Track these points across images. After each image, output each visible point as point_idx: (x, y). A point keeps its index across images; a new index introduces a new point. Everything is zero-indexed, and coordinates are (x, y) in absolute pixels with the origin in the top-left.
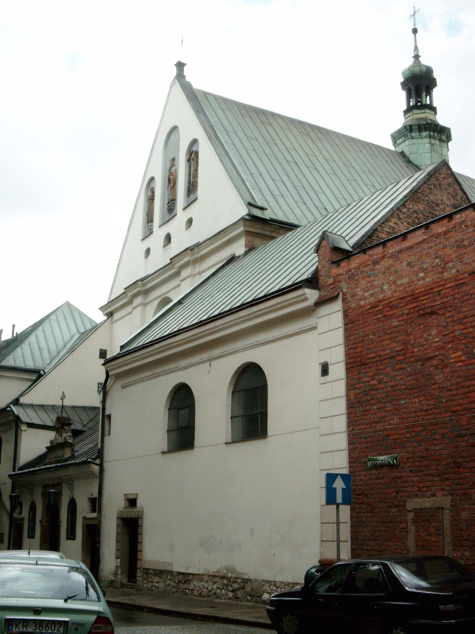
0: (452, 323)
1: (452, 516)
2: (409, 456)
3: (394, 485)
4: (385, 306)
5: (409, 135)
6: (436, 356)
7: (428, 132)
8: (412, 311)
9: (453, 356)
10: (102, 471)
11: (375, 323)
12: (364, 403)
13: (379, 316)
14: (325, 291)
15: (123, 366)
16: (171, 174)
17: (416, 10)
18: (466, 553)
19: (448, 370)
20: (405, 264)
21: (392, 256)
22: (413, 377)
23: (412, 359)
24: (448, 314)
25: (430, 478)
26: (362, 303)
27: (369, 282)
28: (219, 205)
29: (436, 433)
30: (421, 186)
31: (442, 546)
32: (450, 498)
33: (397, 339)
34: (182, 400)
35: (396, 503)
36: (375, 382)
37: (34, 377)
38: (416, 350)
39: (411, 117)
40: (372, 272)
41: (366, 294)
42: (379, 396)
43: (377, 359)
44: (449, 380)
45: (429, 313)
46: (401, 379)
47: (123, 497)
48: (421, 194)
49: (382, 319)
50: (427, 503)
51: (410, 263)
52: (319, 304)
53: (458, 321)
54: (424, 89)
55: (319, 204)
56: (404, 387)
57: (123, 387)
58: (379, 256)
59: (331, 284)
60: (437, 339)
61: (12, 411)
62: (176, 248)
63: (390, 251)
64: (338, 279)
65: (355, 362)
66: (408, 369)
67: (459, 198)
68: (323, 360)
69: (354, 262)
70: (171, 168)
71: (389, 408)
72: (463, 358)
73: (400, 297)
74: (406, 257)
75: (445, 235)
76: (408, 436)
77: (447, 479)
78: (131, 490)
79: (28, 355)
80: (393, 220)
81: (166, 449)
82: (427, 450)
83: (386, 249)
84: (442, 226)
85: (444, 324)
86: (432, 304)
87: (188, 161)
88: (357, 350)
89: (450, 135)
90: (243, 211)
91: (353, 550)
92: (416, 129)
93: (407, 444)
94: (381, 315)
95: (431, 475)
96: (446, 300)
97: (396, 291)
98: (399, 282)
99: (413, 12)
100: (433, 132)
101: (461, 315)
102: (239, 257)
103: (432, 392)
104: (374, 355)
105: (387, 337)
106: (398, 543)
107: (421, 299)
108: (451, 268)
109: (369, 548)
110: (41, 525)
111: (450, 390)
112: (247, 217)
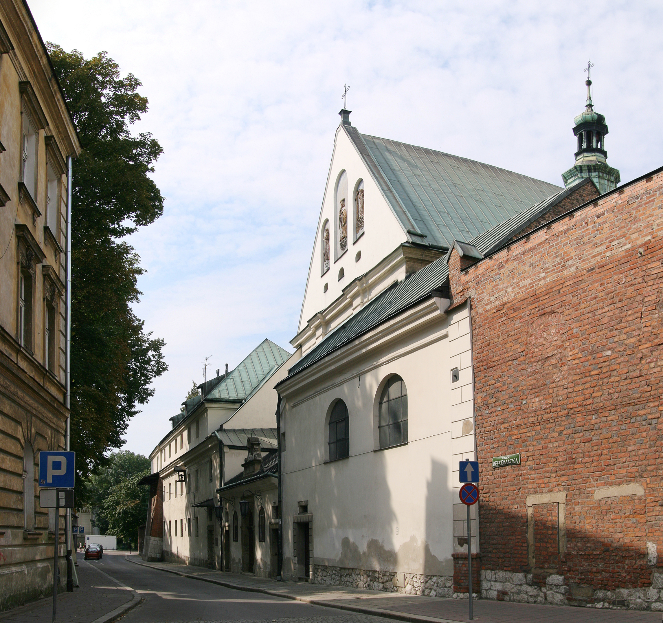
0: (570, 321)
1: (566, 510)
3: (516, 482)
4: (508, 309)
6: (555, 354)
7: (597, 173)
9: (570, 353)
10: (280, 482)
11: (500, 326)
12: (490, 405)
13: (503, 319)
15: (291, 387)
16: (342, 213)
17: (591, 64)
18: (579, 544)
19: (565, 368)
21: (516, 259)
22: (533, 377)
23: (533, 360)
25: (547, 475)
26: (488, 307)
29: (553, 431)
30: (562, 200)
31: (557, 539)
33: (520, 341)
34: (339, 414)
35: (517, 500)
36: (499, 384)
39: (582, 159)
40: (498, 276)
41: (492, 298)
43: (502, 361)
44: (566, 378)
45: (550, 312)
46: (523, 379)
47: (297, 504)
48: (562, 207)
49: (505, 322)
51: (533, 263)
53: (576, 319)
56: (525, 387)
58: (504, 259)
59: (460, 292)
60: (555, 339)
61: (216, 436)
62: (347, 280)
63: (514, 254)
65: (482, 366)
66: (529, 370)
69: (481, 268)
70: (342, 208)
71: (512, 409)
72: (579, 355)
73: (522, 299)
75: (565, 233)
76: (528, 435)
78: (302, 498)
81: (328, 459)
83: (510, 252)
84: (562, 225)
85: (563, 322)
86: (552, 304)
87: (356, 200)
89: (619, 176)
91: (481, 544)
92: (585, 170)
93: (528, 443)
94: (505, 318)
96: (564, 298)
97: (518, 293)
98: (521, 284)
99: (588, 66)
100: (602, 173)
104: (498, 358)
105: (510, 339)
106: (519, 537)
107: (541, 299)
108: (570, 266)
109: (495, 542)
110: (242, 531)
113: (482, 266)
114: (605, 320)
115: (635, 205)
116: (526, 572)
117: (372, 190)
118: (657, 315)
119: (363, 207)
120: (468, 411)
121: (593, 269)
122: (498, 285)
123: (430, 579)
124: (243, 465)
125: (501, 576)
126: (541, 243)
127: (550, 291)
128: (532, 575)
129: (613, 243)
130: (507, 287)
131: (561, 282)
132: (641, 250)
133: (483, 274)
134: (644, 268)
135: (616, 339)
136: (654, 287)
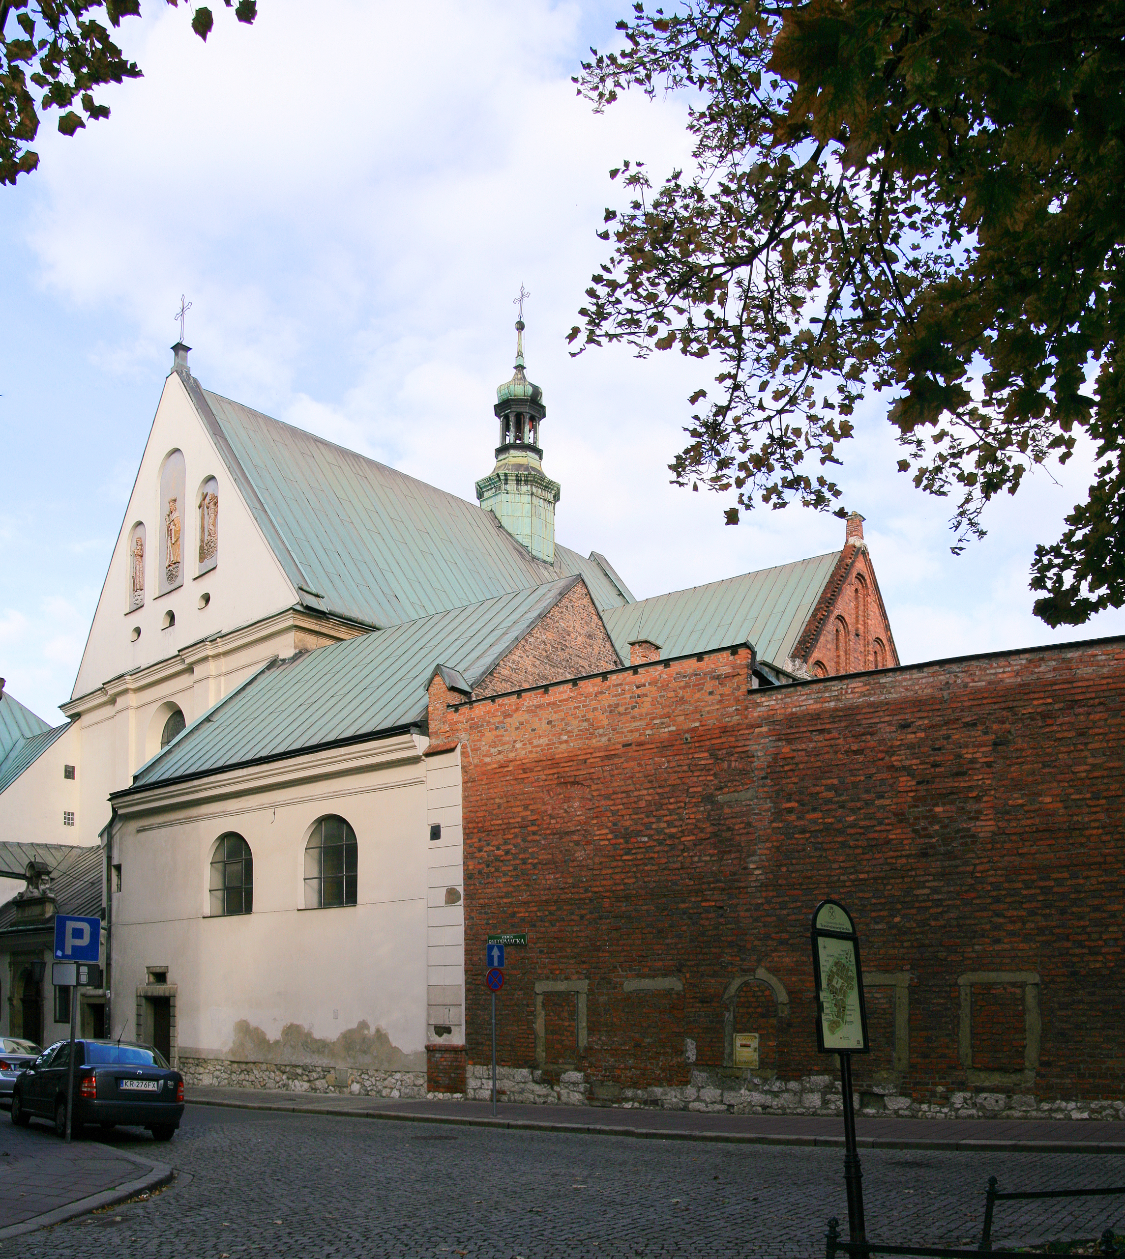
2: (540, 935)
5: (503, 486)
8: (550, 777)
14: (437, 737)
20: (545, 721)
24: (594, 787)
26: (487, 760)
27: (497, 736)
28: (252, 582)
29: (572, 914)
32: (587, 981)
34: (235, 851)
36: (500, 852)
38: (553, 821)
41: (492, 750)
42: (504, 868)
52: (431, 753)
54: (527, 421)
55: (386, 590)
57: (139, 831)
64: (455, 727)
67: (594, 625)
68: (434, 821)
72: (610, 836)
74: (548, 714)
77: (584, 962)
78: (158, 963)
80: (518, 652)
82: (561, 931)
88: (479, 814)
90: (292, 599)
95: (564, 957)
96: (593, 770)
97: (531, 752)
98: (535, 742)
101: (611, 790)
102: (284, 660)
103: (571, 870)
104: (500, 822)
108: (601, 735)
111: (592, 869)
112: (299, 608)
113: (480, 710)
114: (642, 804)
116: (533, 1067)
117: (228, 493)
119: (215, 524)
120: (457, 879)
121: (630, 745)
123: (391, 1075)
126: (564, 700)
132: (687, 736)
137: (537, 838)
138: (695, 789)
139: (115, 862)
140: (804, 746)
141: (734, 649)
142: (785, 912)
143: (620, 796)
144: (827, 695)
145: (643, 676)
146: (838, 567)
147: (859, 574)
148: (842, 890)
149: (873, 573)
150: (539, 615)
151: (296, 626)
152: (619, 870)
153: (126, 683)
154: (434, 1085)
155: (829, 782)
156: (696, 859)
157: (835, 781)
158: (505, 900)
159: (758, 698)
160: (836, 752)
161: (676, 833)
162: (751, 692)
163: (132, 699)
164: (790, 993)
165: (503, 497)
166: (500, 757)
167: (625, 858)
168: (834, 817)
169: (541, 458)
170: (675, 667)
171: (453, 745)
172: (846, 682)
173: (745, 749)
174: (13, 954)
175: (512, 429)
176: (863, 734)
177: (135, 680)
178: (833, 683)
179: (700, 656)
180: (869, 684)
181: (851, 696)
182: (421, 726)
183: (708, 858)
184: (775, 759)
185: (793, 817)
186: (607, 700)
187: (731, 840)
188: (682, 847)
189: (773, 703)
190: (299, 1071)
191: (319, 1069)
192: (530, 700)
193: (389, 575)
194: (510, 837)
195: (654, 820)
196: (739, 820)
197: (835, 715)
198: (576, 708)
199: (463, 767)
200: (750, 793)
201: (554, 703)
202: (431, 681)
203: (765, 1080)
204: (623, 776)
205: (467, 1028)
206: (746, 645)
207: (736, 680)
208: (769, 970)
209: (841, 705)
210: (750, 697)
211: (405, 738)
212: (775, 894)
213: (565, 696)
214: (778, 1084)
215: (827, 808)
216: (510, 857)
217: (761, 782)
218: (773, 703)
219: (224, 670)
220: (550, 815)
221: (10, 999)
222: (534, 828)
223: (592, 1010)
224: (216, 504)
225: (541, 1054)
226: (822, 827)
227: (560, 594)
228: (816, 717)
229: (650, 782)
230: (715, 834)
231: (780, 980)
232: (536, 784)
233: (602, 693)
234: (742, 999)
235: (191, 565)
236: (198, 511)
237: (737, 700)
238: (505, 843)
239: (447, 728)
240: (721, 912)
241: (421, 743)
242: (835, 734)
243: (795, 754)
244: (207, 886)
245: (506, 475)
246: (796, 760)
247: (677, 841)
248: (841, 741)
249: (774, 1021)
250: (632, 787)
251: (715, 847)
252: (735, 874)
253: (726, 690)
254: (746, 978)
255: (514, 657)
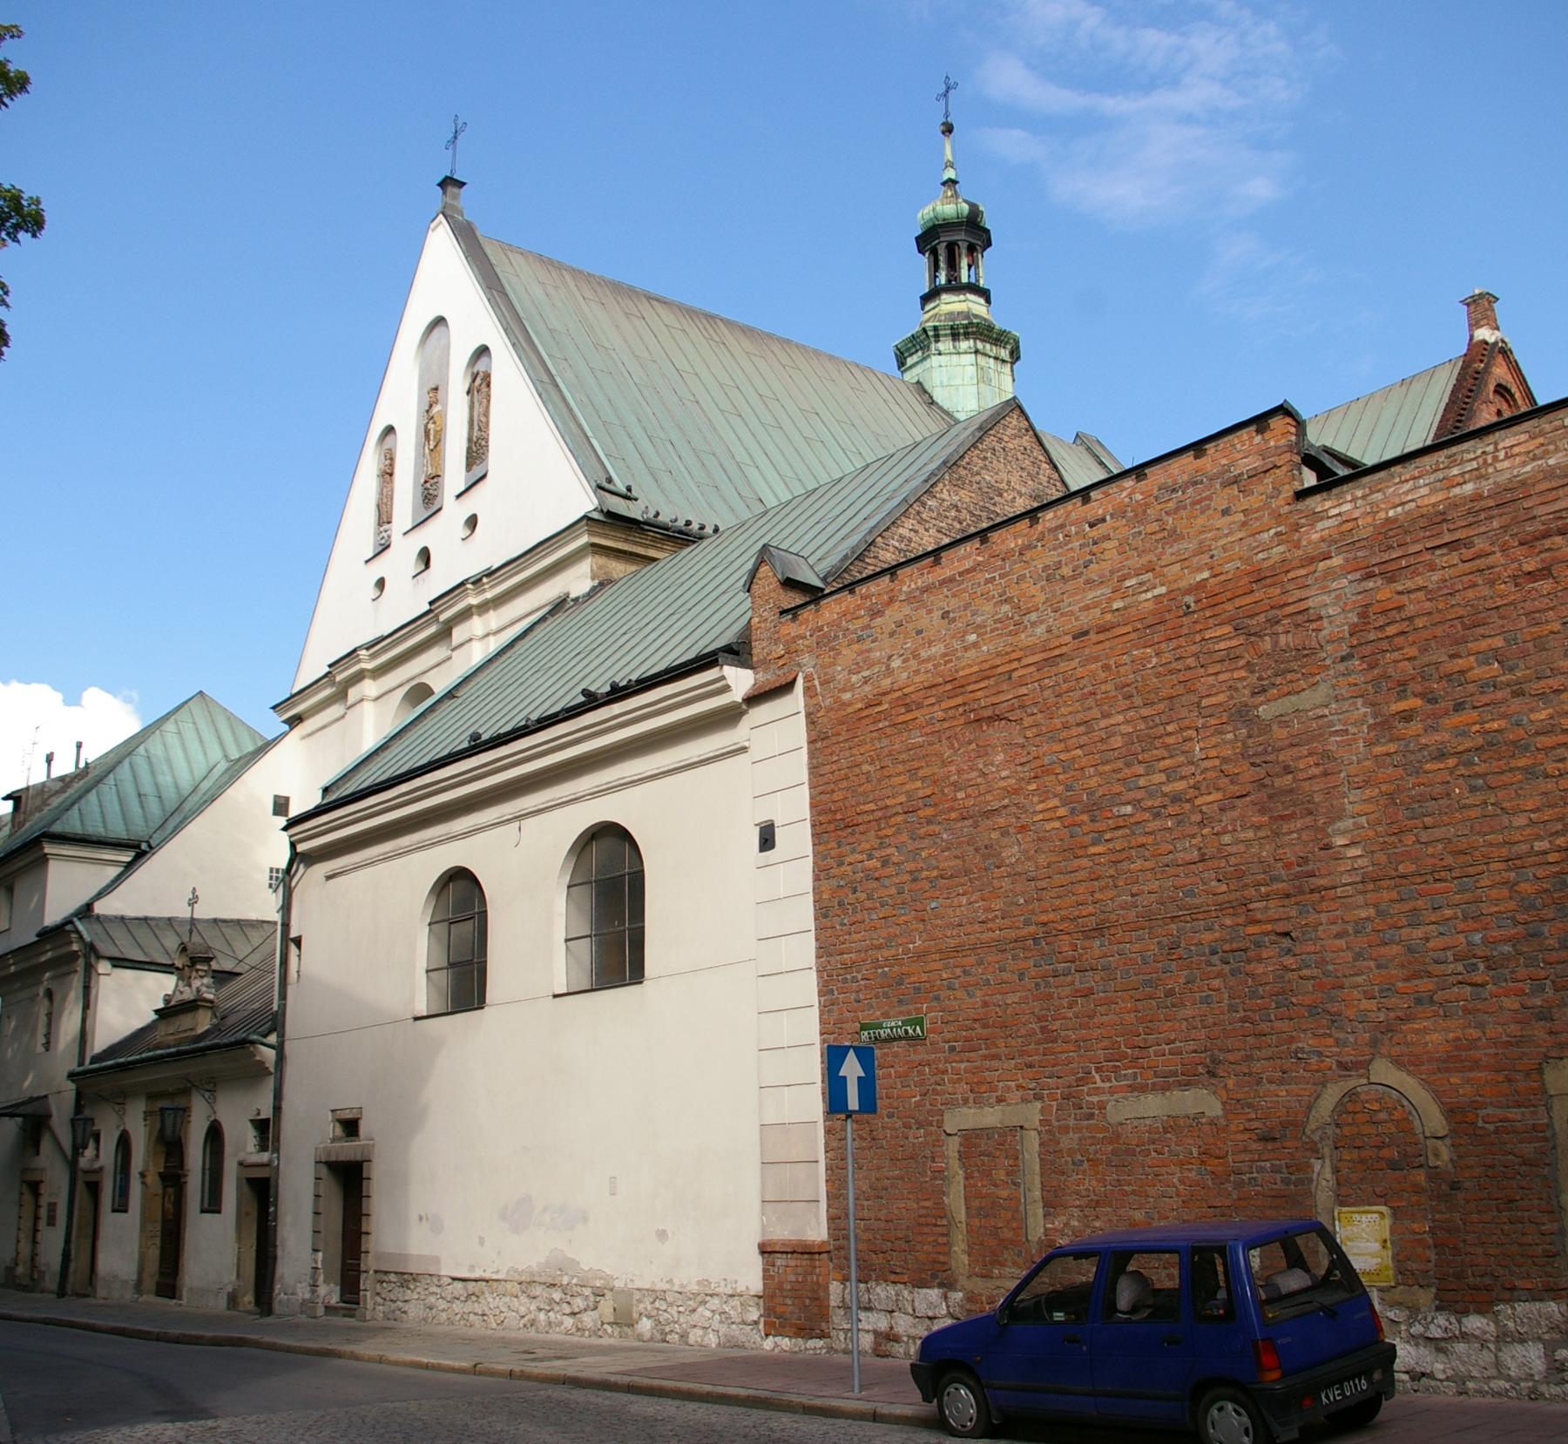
6: (1005, 807)
9: (1040, 807)
13: (881, 725)
20: (937, 614)
26: (847, 696)
27: (860, 653)
36: (874, 863)
37: (127, 857)
38: (961, 795)
41: (854, 678)
49: (888, 731)
50: (991, 1117)
54: (964, 251)
55: (746, 492)
57: (329, 878)
60: (1004, 774)
62: (440, 579)
67: (1044, 480)
68: (763, 817)
72: (1062, 812)
74: (942, 600)
78: (347, 1102)
79: (113, 808)
80: (910, 523)
88: (835, 797)
90: (585, 502)
96: (1024, 690)
97: (917, 672)
98: (924, 654)
102: (576, 600)
106: (927, 1204)
107: (971, 688)
108: (1033, 624)
112: (596, 515)
113: (831, 610)
114: (1117, 742)
115: (1171, 505)
117: (507, 369)
118: (1230, 736)
119: (486, 414)
121: (1086, 633)
122: (869, 651)
123: (704, 1303)
124: (157, 1012)
125: (883, 1295)
126: (968, 571)
127: (989, 673)
128: (961, 1294)
129: (1128, 583)
130: (890, 657)
131: (1014, 656)
132: (1189, 599)
133: (835, 624)
134: (1198, 638)
135: (1142, 782)
136: (1222, 677)
137: (937, 828)
138: (1213, 700)
139: (293, 934)
140: (1419, 581)
141: (1260, 422)
142: (1419, 933)
143: (1075, 731)
144: (1455, 471)
145: (1099, 504)
146: (1461, 378)
147: (1499, 385)
148: (1540, 873)
149: (1524, 382)
150: (944, 463)
151: (593, 545)
152: (1083, 874)
153: (359, 661)
154: (775, 1323)
155: (1483, 645)
156: (1227, 839)
157: (1498, 642)
158: (886, 953)
159: (1315, 503)
160: (1492, 583)
161: (1184, 792)
162: (1301, 495)
163: (369, 687)
164: (1450, 1112)
165: (935, 360)
166: (867, 688)
167: (1093, 850)
168: (1503, 716)
169: (988, 301)
170: (1156, 476)
171: (790, 679)
172: (1491, 438)
173: (1302, 606)
174: (151, 1097)
175: (942, 265)
176: (1546, 535)
177: (373, 656)
178: (1465, 446)
179: (1198, 447)
180: (1542, 434)
181: (1506, 464)
182: (738, 652)
183: (1250, 834)
184: (1363, 615)
185: (1415, 727)
186: (1044, 558)
187: (1291, 791)
188: (1198, 818)
189: (1347, 507)
190: (557, 1296)
191: (587, 1292)
192: (911, 581)
193: (753, 474)
194: (889, 832)
195: (1140, 769)
196: (1304, 750)
197: (1476, 509)
198: (988, 581)
199: (808, 715)
200: (1322, 692)
201: (951, 580)
202: (753, 574)
203: (1414, 1311)
204: (1077, 694)
205: (829, 1206)
206: (1283, 410)
207: (1268, 479)
208: (1398, 1062)
209: (1486, 487)
210: (1300, 506)
211: (712, 674)
212: (1394, 895)
213: (968, 564)
214: (1441, 1320)
215: (1485, 699)
216: (891, 870)
217: (1341, 667)
218: (1347, 507)
219: (494, 626)
220: (954, 784)
221: (142, 1175)
222: (929, 811)
223: (1050, 1166)
224: (488, 385)
225: (960, 1257)
226: (1480, 741)
227: (980, 428)
228: (1437, 519)
229: (1128, 697)
230: (1260, 784)
231: (1426, 1083)
232: (927, 730)
233: (1030, 547)
234: (1347, 1131)
235: (454, 475)
236: (466, 399)
237: (1278, 517)
238: (881, 846)
239: (780, 650)
240: (1286, 942)
241: (740, 681)
242: (1481, 544)
243: (1404, 598)
244: (422, 964)
245: (936, 329)
246: (1411, 609)
247: (1187, 806)
248: (1498, 557)
249: (1420, 1177)
250: (1096, 713)
251: (1262, 811)
252: (1305, 860)
253: (1254, 501)
254: (1352, 1083)
255: (901, 530)
